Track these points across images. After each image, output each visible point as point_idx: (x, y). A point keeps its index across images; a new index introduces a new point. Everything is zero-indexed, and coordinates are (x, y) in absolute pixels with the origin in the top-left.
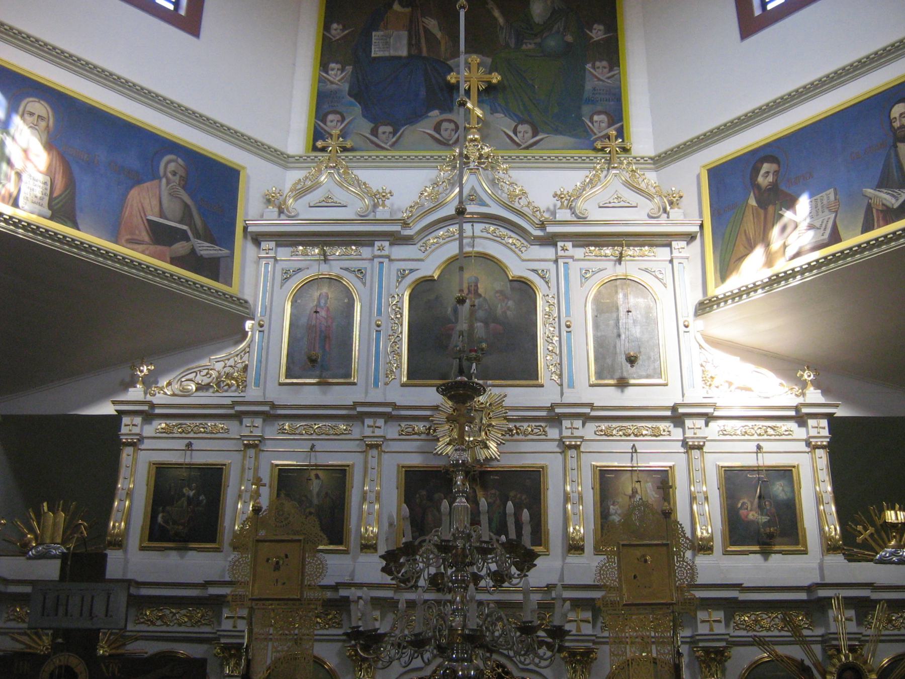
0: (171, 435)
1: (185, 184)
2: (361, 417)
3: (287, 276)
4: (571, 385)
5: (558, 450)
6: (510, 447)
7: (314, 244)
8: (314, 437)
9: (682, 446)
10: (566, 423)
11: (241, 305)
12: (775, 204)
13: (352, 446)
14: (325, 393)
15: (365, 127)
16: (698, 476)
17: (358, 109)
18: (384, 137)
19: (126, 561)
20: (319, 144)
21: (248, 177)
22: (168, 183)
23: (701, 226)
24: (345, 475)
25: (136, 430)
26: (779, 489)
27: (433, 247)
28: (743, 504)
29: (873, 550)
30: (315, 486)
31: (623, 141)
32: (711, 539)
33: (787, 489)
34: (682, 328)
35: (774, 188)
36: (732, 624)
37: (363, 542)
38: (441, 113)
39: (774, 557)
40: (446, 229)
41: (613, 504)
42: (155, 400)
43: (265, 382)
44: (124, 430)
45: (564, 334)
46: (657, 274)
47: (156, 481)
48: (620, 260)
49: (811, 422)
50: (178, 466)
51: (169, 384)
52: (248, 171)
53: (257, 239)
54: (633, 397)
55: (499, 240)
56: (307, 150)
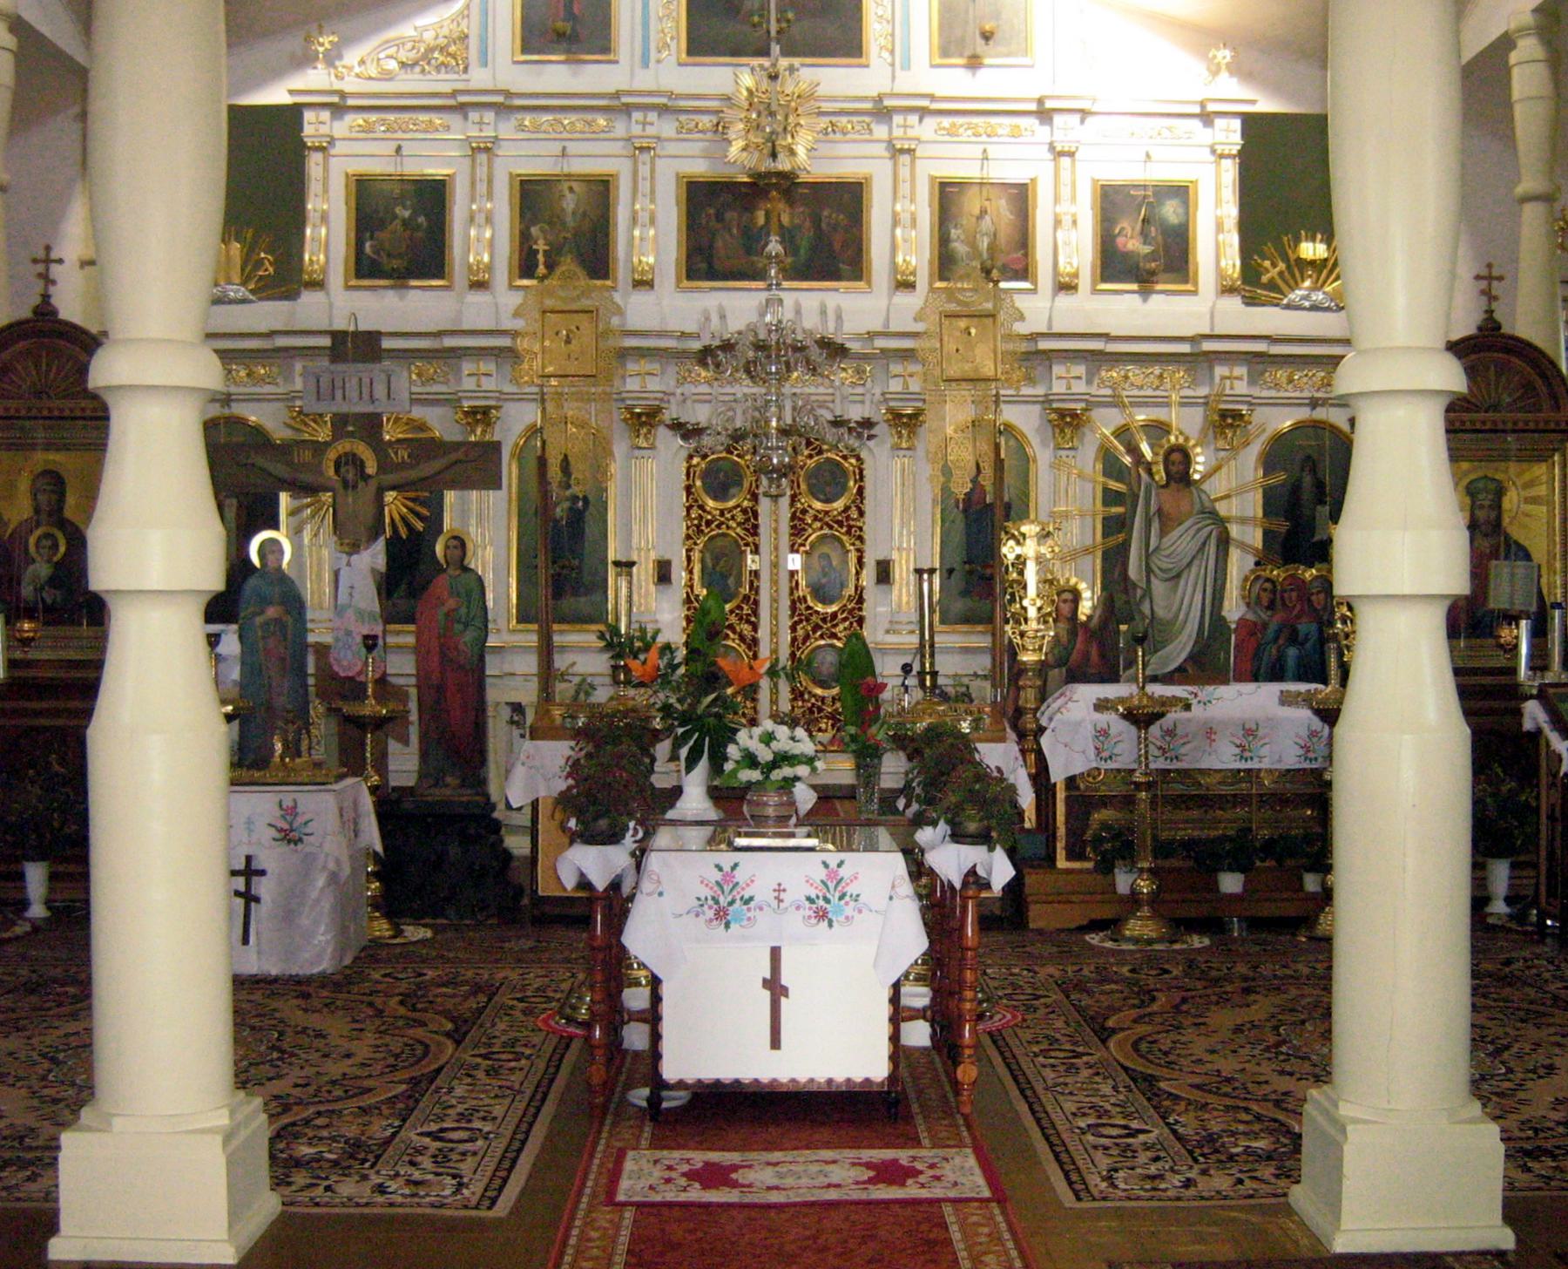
2: (628, 109)
4: (907, 66)
6: (824, 149)
8: (565, 135)
10: (898, 119)
13: (616, 148)
16: (1065, 192)
19: (331, 305)
24: (607, 190)
25: (324, 130)
26: (1170, 211)
28: (1122, 229)
29: (1282, 293)
30: (569, 203)
32: (1076, 275)
33: (1181, 211)
36: (1096, 381)
37: (636, 276)
39: (1155, 298)
41: (956, 227)
42: (347, 88)
43: (494, 60)
47: (357, 204)
49: (1219, 123)
50: (387, 179)
51: (362, 62)
54: (992, 82)
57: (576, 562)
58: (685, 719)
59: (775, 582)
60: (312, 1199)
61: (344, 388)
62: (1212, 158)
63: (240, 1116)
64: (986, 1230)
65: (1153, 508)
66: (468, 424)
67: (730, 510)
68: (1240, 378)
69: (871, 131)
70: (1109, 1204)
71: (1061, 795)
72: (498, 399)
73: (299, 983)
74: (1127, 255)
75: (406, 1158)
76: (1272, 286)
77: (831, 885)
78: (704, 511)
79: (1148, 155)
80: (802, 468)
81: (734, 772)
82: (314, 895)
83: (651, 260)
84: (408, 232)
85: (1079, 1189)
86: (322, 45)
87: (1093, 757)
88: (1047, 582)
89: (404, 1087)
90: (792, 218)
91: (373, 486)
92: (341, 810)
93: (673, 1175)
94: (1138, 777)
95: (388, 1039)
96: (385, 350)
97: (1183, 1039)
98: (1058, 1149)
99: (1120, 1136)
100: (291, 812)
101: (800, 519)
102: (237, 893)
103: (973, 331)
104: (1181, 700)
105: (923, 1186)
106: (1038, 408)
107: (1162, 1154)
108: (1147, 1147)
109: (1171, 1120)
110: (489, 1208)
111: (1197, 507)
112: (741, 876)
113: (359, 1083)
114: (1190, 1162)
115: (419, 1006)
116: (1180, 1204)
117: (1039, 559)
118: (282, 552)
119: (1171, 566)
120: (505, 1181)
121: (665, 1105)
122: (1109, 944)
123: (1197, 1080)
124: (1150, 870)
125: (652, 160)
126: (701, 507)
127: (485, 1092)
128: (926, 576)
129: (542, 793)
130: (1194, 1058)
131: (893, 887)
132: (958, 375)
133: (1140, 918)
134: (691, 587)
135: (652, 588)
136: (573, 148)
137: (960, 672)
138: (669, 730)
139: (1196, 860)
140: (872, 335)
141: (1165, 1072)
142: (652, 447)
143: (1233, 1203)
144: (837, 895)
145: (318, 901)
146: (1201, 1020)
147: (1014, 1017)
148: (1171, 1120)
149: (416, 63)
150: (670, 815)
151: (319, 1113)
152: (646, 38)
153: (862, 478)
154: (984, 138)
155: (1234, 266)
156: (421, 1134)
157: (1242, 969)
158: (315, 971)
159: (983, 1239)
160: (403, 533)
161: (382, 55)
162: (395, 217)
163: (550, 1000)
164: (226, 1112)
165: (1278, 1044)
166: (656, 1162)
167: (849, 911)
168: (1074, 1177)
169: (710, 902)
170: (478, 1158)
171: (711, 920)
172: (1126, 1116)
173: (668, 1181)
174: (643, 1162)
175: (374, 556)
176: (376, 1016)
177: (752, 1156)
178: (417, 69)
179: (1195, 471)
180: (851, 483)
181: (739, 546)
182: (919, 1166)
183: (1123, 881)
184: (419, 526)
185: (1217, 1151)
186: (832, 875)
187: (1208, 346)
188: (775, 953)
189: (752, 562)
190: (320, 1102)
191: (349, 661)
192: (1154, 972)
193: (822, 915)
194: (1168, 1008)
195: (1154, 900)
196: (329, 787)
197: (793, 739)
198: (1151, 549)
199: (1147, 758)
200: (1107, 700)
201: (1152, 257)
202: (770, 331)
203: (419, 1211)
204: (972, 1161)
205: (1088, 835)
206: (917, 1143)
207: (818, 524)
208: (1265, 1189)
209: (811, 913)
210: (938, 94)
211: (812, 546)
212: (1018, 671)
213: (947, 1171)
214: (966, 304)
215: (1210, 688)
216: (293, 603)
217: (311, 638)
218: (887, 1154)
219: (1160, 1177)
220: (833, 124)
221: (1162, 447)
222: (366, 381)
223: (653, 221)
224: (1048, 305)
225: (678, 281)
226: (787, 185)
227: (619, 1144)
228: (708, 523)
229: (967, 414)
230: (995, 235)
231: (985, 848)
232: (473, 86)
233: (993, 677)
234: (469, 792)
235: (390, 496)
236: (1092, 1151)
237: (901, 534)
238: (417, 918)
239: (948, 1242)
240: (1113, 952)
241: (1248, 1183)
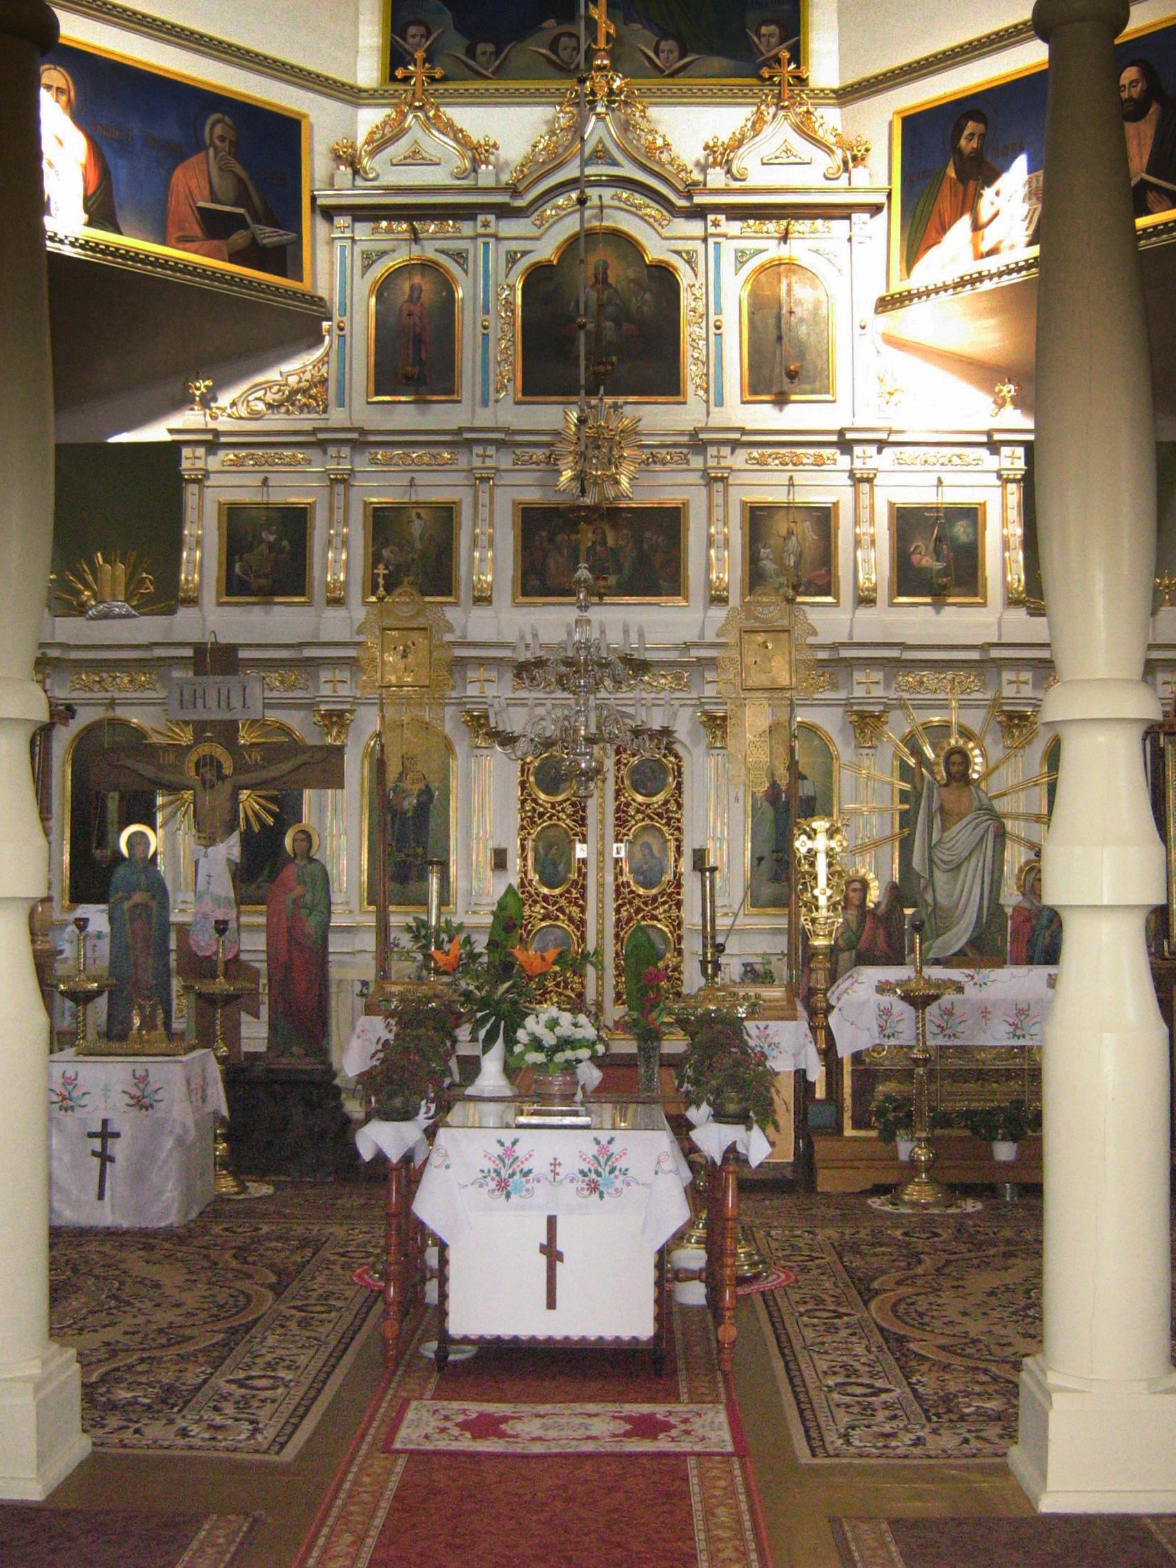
0: (241, 469)
1: (237, 151)
2: (469, 443)
4: (720, 402)
5: (702, 482)
6: (645, 480)
7: (399, 218)
8: (413, 468)
9: (850, 477)
10: (712, 451)
11: (315, 303)
12: (977, 180)
13: (459, 478)
14: (423, 413)
15: (457, 45)
16: (865, 514)
17: (448, 16)
18: (483, 59)
19: (204, 619)
20: (399, 73)
21: (311, 126)
22: (216, 154)
23: (889, 196)
24: (450, 518)
26: (960, 530)
27: (551, 221)
28: (916, 547)
30: (417, 528)
31: (798, 67)
32: (875, 590)
33: (970, 530)
34: (858, 330)
35: (978, 156)
36: (894, 686)
38: (558, 24)
40: (565, 196)
41: (765, 547)
42: (221, 428)
44: (186, 464)
45: (712, 338)
46: (831, 257)
48: (785, 238)
49: (1005, 451)
50: (257, 506)
51: (234, 404)
52: (312, 119)
53: (329, 213)
55: (634, 210)
56: (383, 82)
57: (420, 850)
58: (484, 1003)
59: (601, 869)
60: (121, 1441)
61: (204, 698)
62: (998, 483)
63: (53, 1366)
64: (722, 1483)
65: (935, 806)
66: (325, 725)
67: (561, 803)
68: (1025, 683)
69: (688, 463)
70: (843, 1461)
71: (847, 1068)
72: (353, 703)
73: (146, 1235)
74: (922, 572)
75: (212, 1404)
77: (602, 1161)
78: (537, 804)
79: (940, 480)
80: (625, 765)
81: (522, 1054)
82: (163, 1156)
83: (490, 578)
84: (273, 555)
85: (815, 1442)
86: (198, 389)
87: (877, 1035)
88: (834, 874)
89: (222, 1336)
90: (616, 540)
91: (228, 787)
92: (188, 1081)
93: (448, 1424)
95: (216, 1289)
96: (242, 660)
97: (940, 1301)
98: (804, 1406)
99: (865, 1395)
100: (143, 1080)
101: (624, 812)
102: (94, 1153)
103: (770, 646)
104: (954, 982)
105: (673, 1440)
106: (841, 709)
107: (900, 1413)
108: (886, 1406)
109: (914, 1380)
110: (278, 1453)
111: (976, 803)
112: (520, 1151)
113: (181, 1332)
114: (924, 1421)
115: (250, 1259)
116: (906, 1462)
117: (830, 854)
119: (950, 858)
120: (296, 1426)
121: (451, 1358)
122: (889, 1208)
123: (944, 1341)
124: (927, 1140)
125: (491, 489)
126: (535, 801)
127: (294, 1342)
128: (708, 874)
130: (946, 1320)
131: (659, 1162)
132: (757, 684)
133: (919, 1184)
134: (525, 873)
135: (490, 873)
136: (421, 479)
137: (768, 951)
138: (472, 1012)
139: (972, 1129)
140: (688, 646)
141: (917, 1334)
143: (958, 1462)
144: (608, 1169)
145: (165, 1162)
146: (960, 1283)
147: (788, 1277)
148: (914, 1380)
149: (281, 405)
150: (470, 1091)
151: (142, 1360)
153: (680, 774)
154: (790, 467)
155: (1019, 580)
156: (229, 1381)
157: (1007, 1233)
158: (162, 1225)
159: (718, 1492)
160: (256, 828)
161: (251, 398)
162: (262, 541)
163: (369, 1254)
164: (38, 1362)
165: (1028, 1307)
166: (435, 1412)
167: (618, 1183)
168: (814, 1434)
169: (493, 1175)
170: (276, 1405)
171: (493, 1191)
172: (872, 1375)
173: (442, 1430)
174: (424, 1412)
175: (230, 848)
176: (210, 1268)
177: (524, 1408)
178: (283, 409)
179: (974, 771)
180: (671, 779)
181: (568, 836)
182: (672, 1420)
183: (905, 1148)
184: (270, 821)
185: (949, 1411)
187: (995, 653)
188: (552, 1222)
189: (581, 851)
190: (144, 1349)
191: (205, 942)
192: (924, 1236)
193: (594, 1187)
194: (932, 1271)
195: (930, 1166)
196: (177, 1058)
197: (575, 1025)
198: (934, 842)
199: (924, 1036)
200: (887, 982)
201: (944, 572)
202: (578, 649)
203: (215, 1454)
204: (722, 1417)
206: (676, 1399)
207: (640, 816)
208: (988, 1449)
209: (584, 1185)
210: (749, 427)
211: (635, 836)
212: (811, 954)
213: (697, 1425)
214: (764, 621)
215: (985, 971)
216: (158, 890)
217: (175, 917)
218: (645, 1408)
219: (893, 1435)
220: (653, 456)
221: (942, 749)
222: (224, 691)
224: (849, 616)
225: (514, 596)
226: (611, 514)
227: (404, 1394)
228: (541, 815)
229: (764, 723)
230: (800, 555)
231: (742, 1128)
232: (331, 424)
233: (790, 955)
234: (312, 1060)
235: (244, 794)
236: (833, 1408)
237: (715, 823)
238: (262, 1174)
239: (686, 1495)
240: (889, 1215)
241: (974, 1443)
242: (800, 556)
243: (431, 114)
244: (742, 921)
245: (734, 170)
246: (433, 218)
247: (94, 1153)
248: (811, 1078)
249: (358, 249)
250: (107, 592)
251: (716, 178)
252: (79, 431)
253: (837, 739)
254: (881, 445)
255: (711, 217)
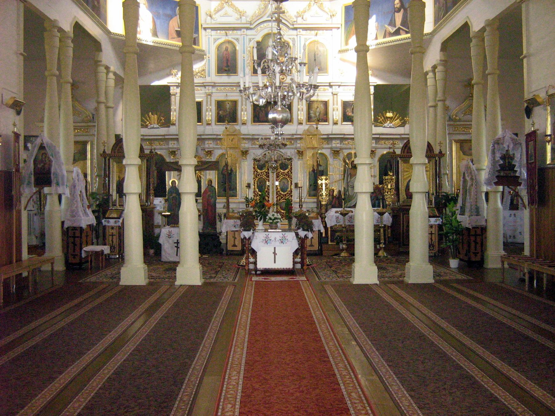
3: (215, 40)
16: (335, 103)
24: (236, 103)
30: (228, 106)
32: (338, 121)
53: (205, 29)
58: (259, 212)
59: (273, 188)
65: (349, 173)
71: (329, 229)
76: (381, 123)
94: (343, 226)
102: (176, 247)
106: (329, 150)
112: (269, 236)
117: (326, 185)
118: (176, 183)
126: (257, 172)
129: (228, 230)
136: (228, 94)
140: (293, 135)
142: (246, 159)
152: (244, 64)
167: (286, 241)
186: (284, 236)
188: (275, 248)
193: (282, 242)
205: (335, 238)
212: (321, 205)
223: (246, 110)
225: (252, 123)
228: (258, 175)
232: (207, 81)
242: (320, 113)
243: (230, 4)
244: (306, 200)
245: (304, 18)
246: (230, 30)
247: (176, 247)
248: (321, 232)
249: (213, 37)
250: (153, 122)
251: (300, 20)
252: (143, 81)
253: (329, 157)
254: (339, 86)
255: (298, 30)
